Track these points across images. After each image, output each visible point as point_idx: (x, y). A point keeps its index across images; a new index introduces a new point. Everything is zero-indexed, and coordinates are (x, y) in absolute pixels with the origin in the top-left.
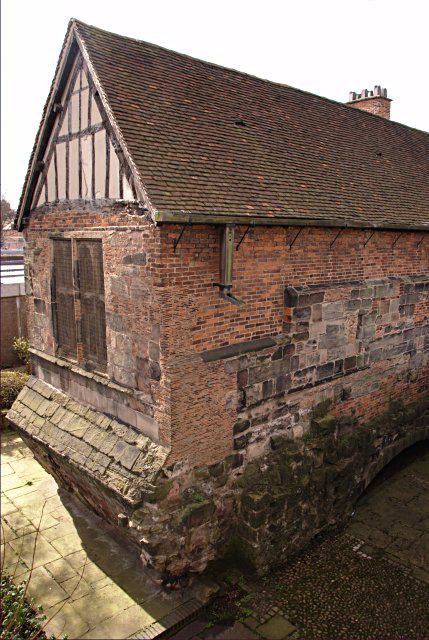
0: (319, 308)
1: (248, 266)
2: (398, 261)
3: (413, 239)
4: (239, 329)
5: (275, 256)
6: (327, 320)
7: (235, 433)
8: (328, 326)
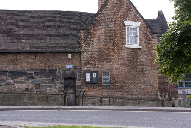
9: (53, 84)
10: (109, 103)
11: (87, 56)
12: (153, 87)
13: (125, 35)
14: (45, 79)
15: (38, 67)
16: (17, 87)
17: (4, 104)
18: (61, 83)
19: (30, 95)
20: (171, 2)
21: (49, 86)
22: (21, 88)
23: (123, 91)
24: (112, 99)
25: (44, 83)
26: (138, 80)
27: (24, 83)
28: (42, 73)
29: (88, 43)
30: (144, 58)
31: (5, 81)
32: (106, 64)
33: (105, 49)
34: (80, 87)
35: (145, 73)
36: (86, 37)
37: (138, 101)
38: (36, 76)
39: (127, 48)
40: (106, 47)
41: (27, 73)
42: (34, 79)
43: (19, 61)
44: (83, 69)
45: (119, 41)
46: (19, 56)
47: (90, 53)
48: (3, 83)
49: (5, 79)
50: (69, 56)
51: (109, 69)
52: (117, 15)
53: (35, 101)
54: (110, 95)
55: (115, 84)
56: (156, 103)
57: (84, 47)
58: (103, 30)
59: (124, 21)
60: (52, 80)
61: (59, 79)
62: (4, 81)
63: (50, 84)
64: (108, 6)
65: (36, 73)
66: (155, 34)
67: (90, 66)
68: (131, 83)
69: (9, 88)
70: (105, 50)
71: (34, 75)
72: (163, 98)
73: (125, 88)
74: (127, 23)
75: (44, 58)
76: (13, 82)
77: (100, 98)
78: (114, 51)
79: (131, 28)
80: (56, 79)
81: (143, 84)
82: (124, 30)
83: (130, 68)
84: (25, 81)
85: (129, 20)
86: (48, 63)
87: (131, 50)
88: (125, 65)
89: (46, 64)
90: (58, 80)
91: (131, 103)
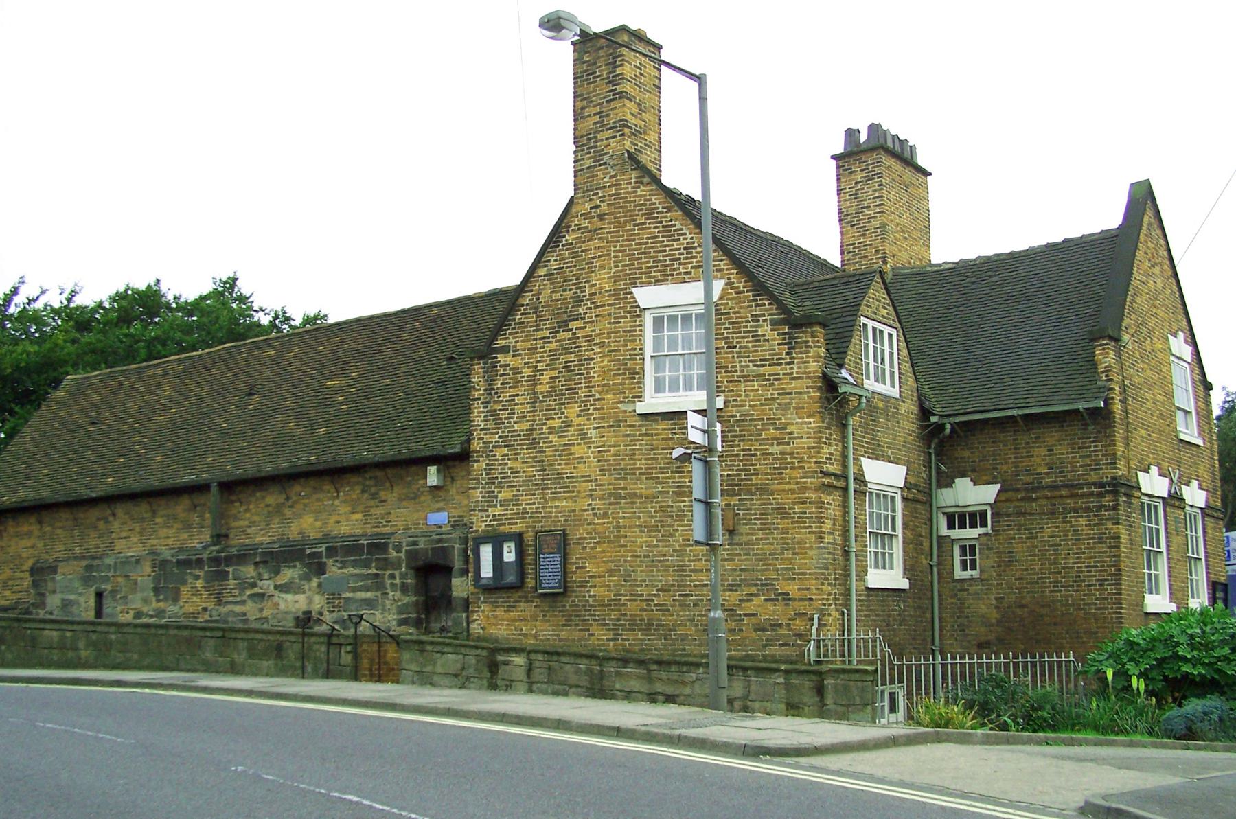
0: (53, 580)
1: (12, 543)
2: (163, 532)
3: (185, 501)
4: (7, 593)
5: (29, 534)
6: (62, 592)
7: (880, 330)
8: (63, 600)
9: (379, 594)
10: (529, 676)
11: (490, 468)
12: (786, 598)
13: (638, 355)
14: (356, 575)
15: (345, 529)
16: (282, 606)
17: (146, 663)
18: (404, 589)
19: (223, 637)
20: (28, 298)
21: (366, 600)
22: (293, 610)
23: (619, 620)
24: (540, 657)
25: (355, 590)
26: (699, 565)
27: (298, 590)
28: (348, 550)
29: (493, 413)
30: (738, 455)
31: (254, 585)
32: (553, 499)
33: (552, 430)
34: (466, 603)
35: (744, 529)
36: (489, 391)
37: (674, 668)
38: (330, 562)
39: (644, 416)
40: (556, 423)
41: (308, 552)
42: (325, 573)
43: (294, 510)
44: (474, 529)
45: (605, 388)
46: (296, 488)
47: (498, 453)
48: (248, 592)
49: (252, 578)
50: (433, 476)
51: (566, 521)
52: (603, 267)
53: (241, 657)
54: (567, 640)
55: (586, 586)
56: (781, 680)
57: (482, 430)
58: (549, 347)
59: (634, 290)
60: (376, 575)
61: (397, 573)
62: (250, 584)
63: (369, 595)
64: (569, 238)
65: (331, 551)
66: (801, 326)
67: (498, 511)
68: (662, 579)
69: (261, 610)
70: (554, 438)
71: (324, 560)
72: (824, 656)
73: (633, 608)
74: (646, 296)
75: (363, 491)
76: (272, 587)
77: (485, 653)
78: (584, 436)
79: (673, 319)
80: (388, 572)
81: (733, 587)
82: (635, 332)
83: (662, 509)
84: (303, 582)
85: (663, 281)
86: (373, 511)
87: (664, 424)
88: (634, 495)
89: (367, 514)
90: (392, 576)
91: (639, 677)
